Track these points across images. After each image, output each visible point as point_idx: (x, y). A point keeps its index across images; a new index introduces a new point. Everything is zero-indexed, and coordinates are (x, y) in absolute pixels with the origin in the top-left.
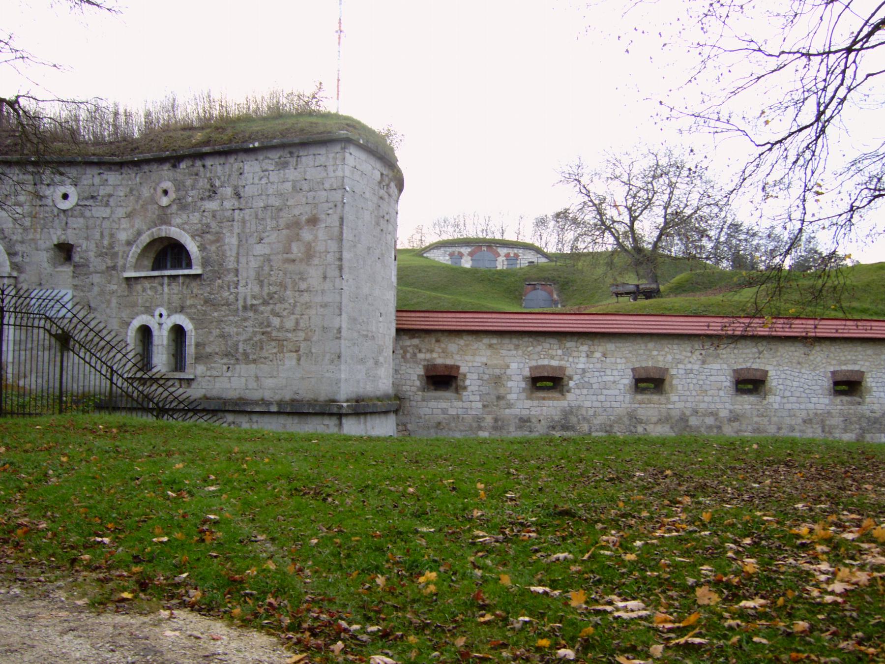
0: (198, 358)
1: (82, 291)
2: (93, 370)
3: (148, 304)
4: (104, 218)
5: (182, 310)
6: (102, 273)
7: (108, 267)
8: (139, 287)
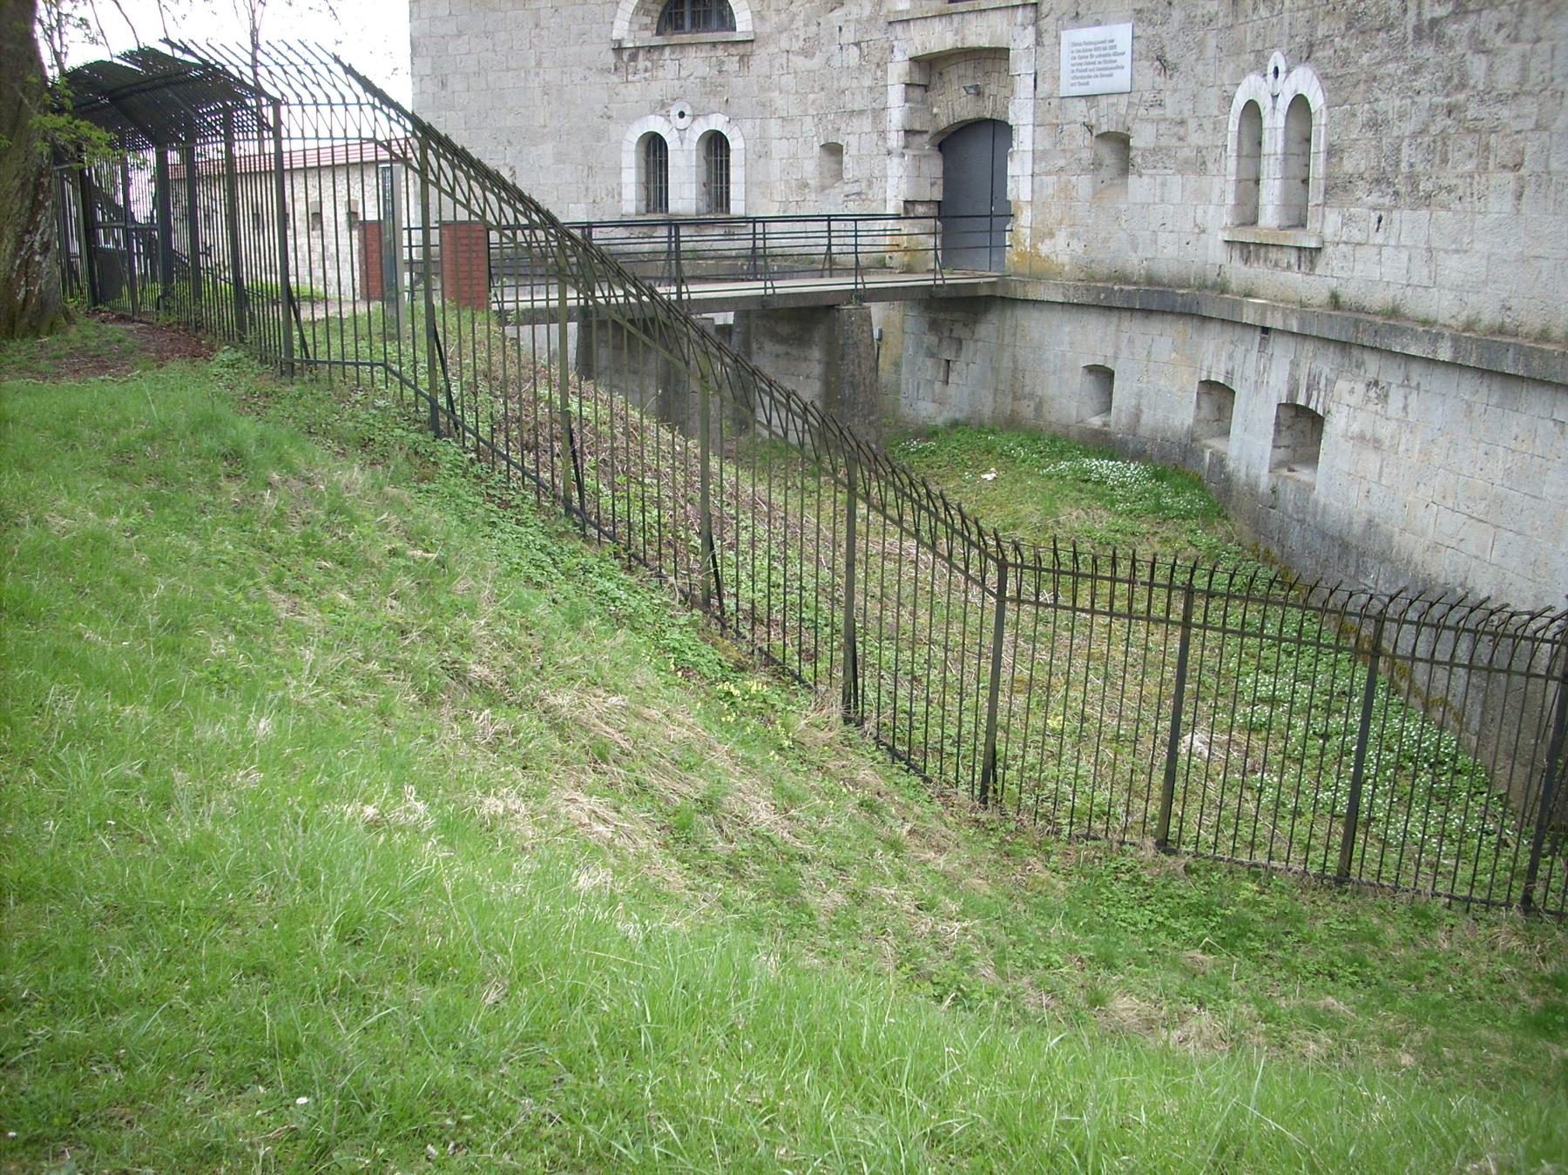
2: (409, 375)
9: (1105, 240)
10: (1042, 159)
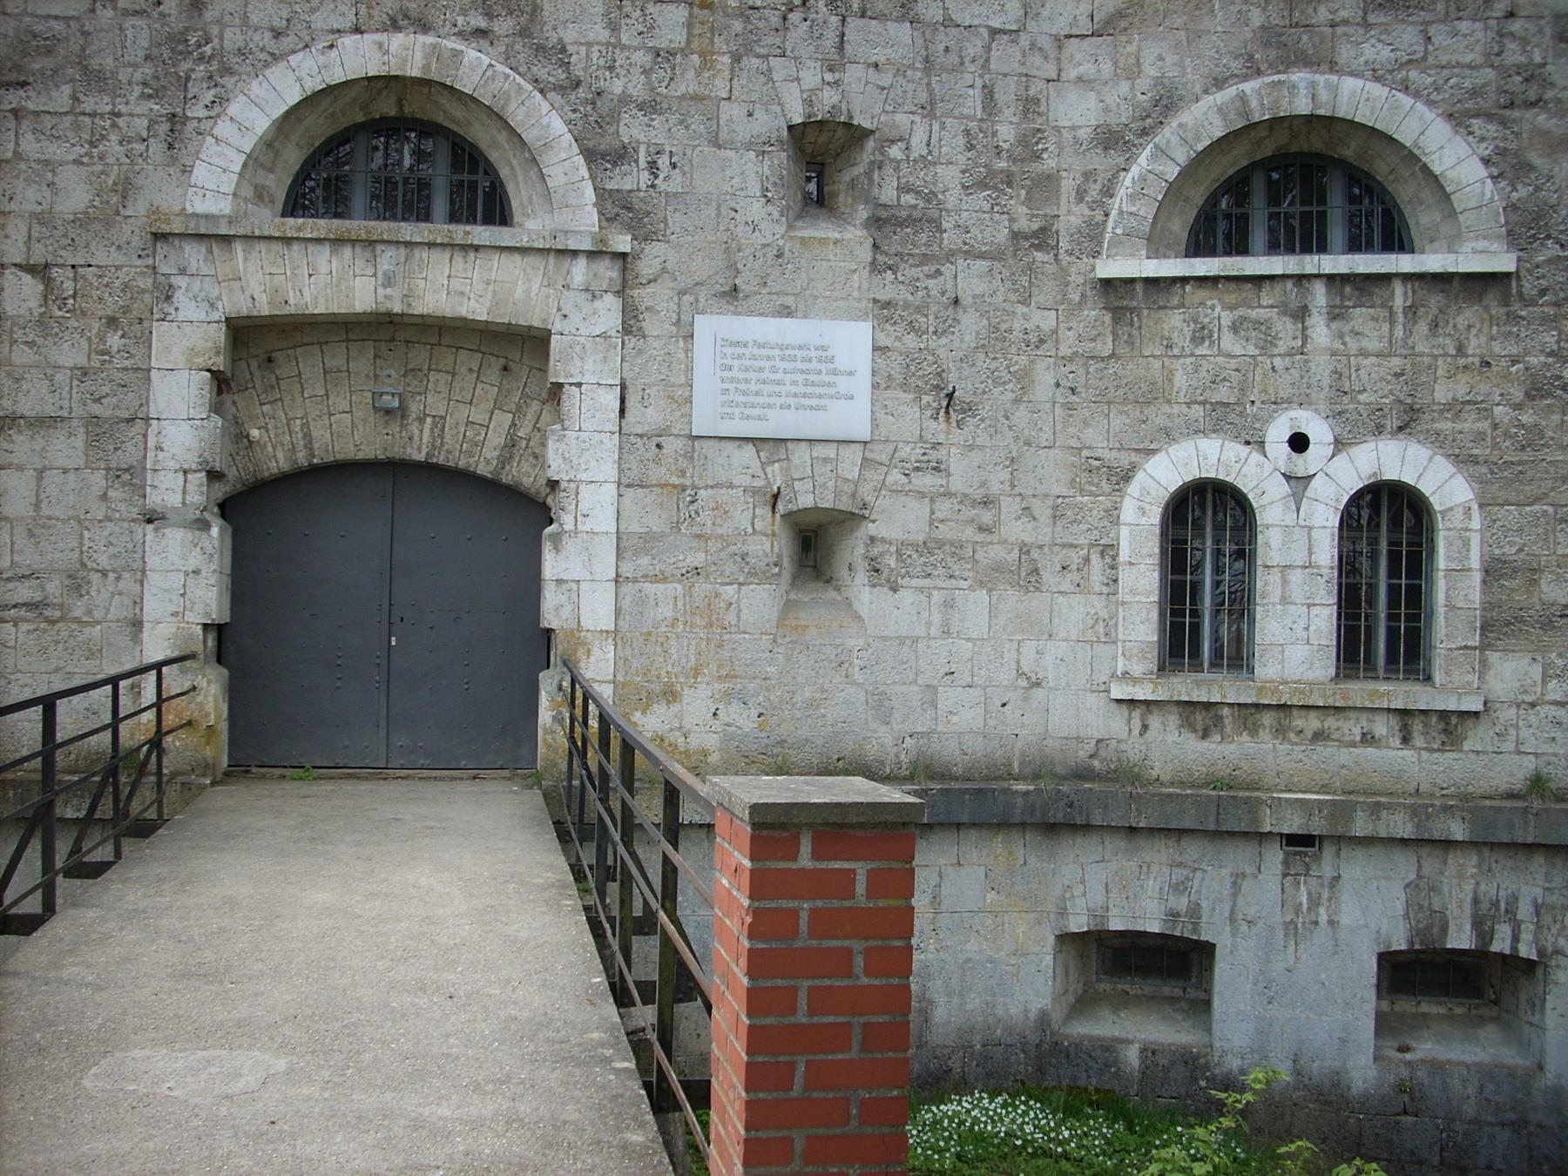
0: (1497, 627)
1: (912, 327)
3: (1223, 394)
4: (994, 32)
5: (1408, 420)
6: (994, 256)
7: (1015, 236)
8: (1175, 322)
9: (811, 704)
10: (636, 553)
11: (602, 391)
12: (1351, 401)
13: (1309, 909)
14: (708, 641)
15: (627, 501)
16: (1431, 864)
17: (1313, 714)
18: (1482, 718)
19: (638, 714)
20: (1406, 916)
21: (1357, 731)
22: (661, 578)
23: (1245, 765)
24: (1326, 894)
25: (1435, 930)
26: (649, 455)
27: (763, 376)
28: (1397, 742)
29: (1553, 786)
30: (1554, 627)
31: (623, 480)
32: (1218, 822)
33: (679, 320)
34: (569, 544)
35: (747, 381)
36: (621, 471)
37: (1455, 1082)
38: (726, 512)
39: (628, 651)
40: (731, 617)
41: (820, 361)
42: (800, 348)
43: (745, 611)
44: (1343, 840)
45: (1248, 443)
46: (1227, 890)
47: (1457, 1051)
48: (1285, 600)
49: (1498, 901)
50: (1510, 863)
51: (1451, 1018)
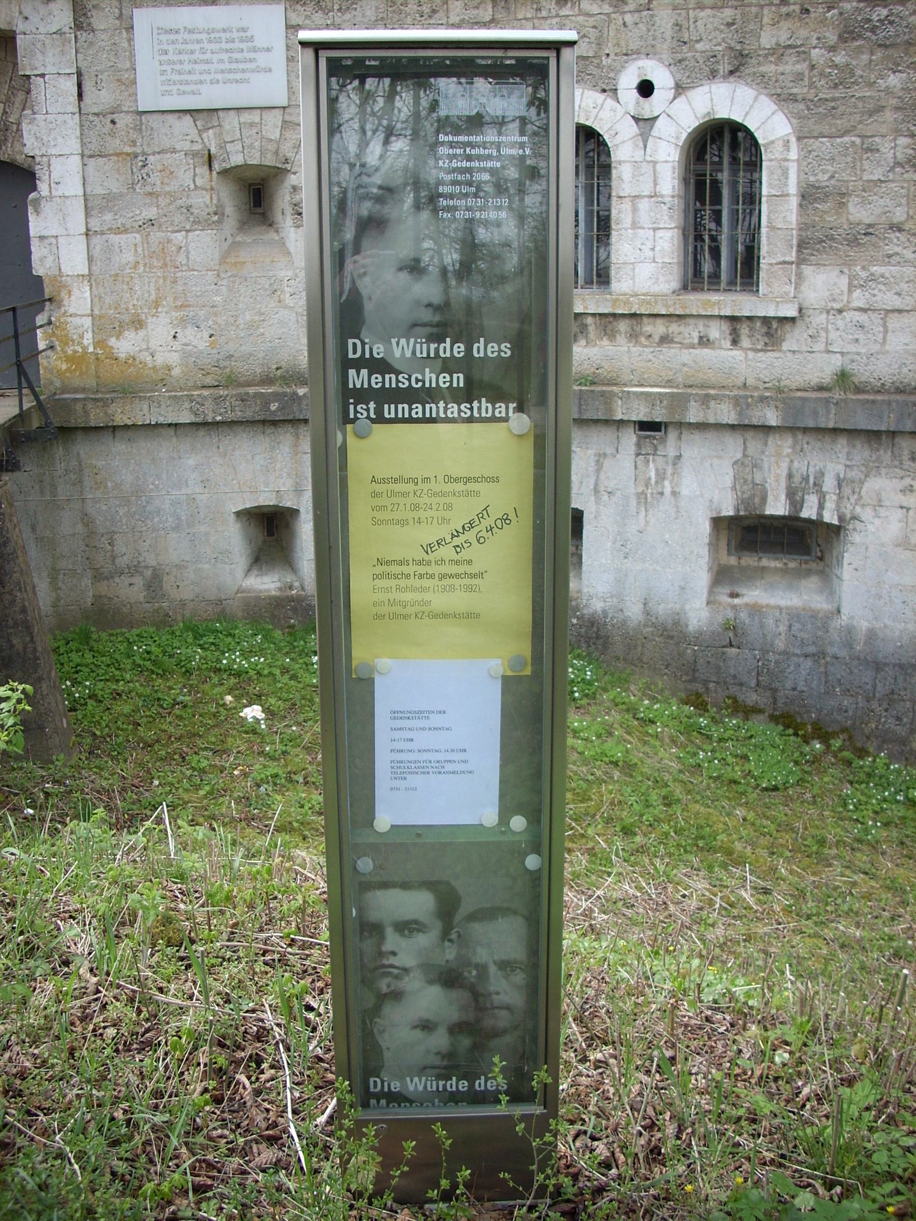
0: (810, 245)
5: (737, 64)
9: (251, 326)
10: (102, 210)
11: (62, 80)
12: (690, 50)
13: (657, 482)
14: (165, 279)
15: (90, 169)
16: (754, 446)
17: (659, 321)
18: (798, 323)
19: (113, 340)
20: (734, 488)
21: (695, 335)
22: (119, 231)
23: (606, 366)
24: (670, 470)
25: (757, 500)
26: (105, 130)
27: (194, 57)
28: (727, 344)
29: (856, 380)
30: (859, 244)
31: (87, 152)
32: (580, 412)
33: (121, 14)
34: (46, 207)
35: (181, 62)
36: (83, 144)
37: (770, 622)
38: (172, 173)
39: (101, 290)
40: (182, 258)
41: (241, 41)
42: (224, 31)
43: (193, 252)
44: (681, 425)
45: (604, 91)
46: (592, 468)
47: (777, 597)
48: (635, 226)
49: (808, 476)
50: (819, 444)
51: (785, 571)
